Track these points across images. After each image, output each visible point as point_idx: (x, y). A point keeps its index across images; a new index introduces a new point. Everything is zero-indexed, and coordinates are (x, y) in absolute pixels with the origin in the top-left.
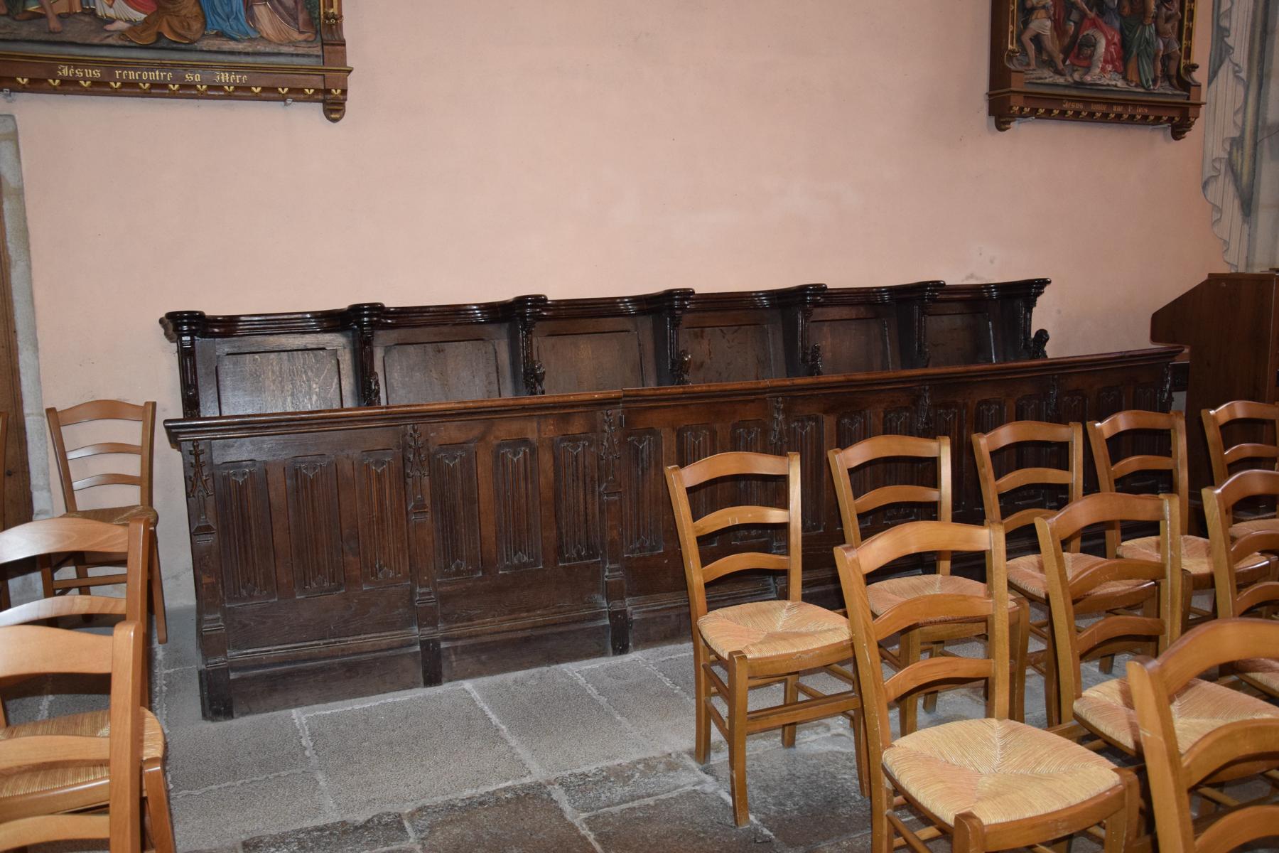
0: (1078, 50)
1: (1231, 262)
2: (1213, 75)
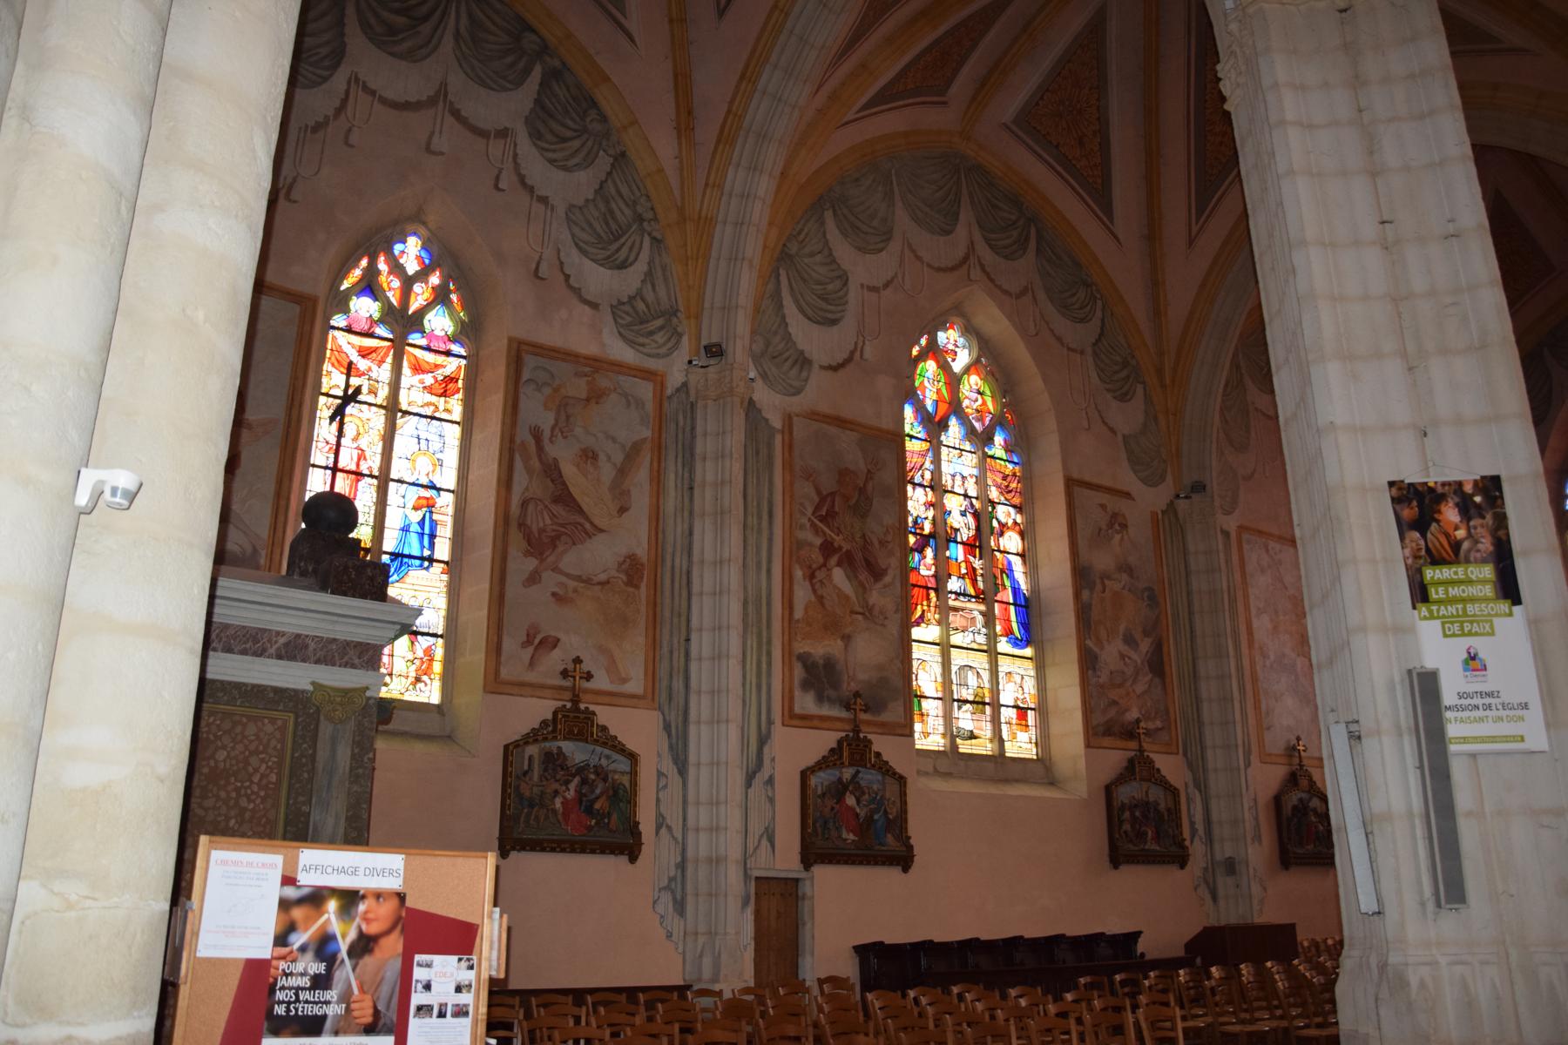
0: (1141, 836)
1: (1212, 922)
2: (1192, 842)
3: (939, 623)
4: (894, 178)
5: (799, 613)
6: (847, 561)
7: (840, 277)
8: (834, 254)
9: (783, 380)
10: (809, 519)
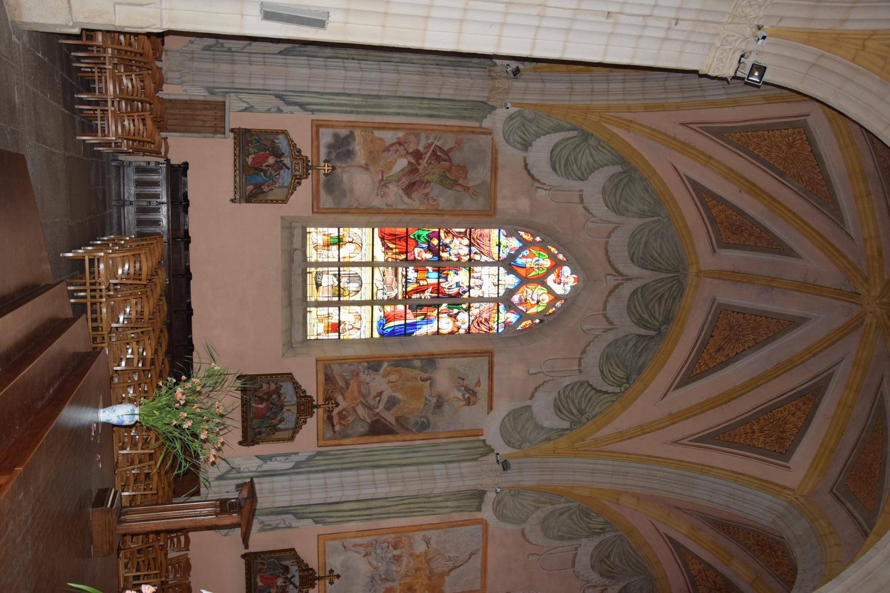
3: (386, 261)
4: (656, 218)
5: (377, 134)
6: (413, 169)
7: (583, 174)
8: (596, 171)
9: (512, 131)
10: (433, 143)
